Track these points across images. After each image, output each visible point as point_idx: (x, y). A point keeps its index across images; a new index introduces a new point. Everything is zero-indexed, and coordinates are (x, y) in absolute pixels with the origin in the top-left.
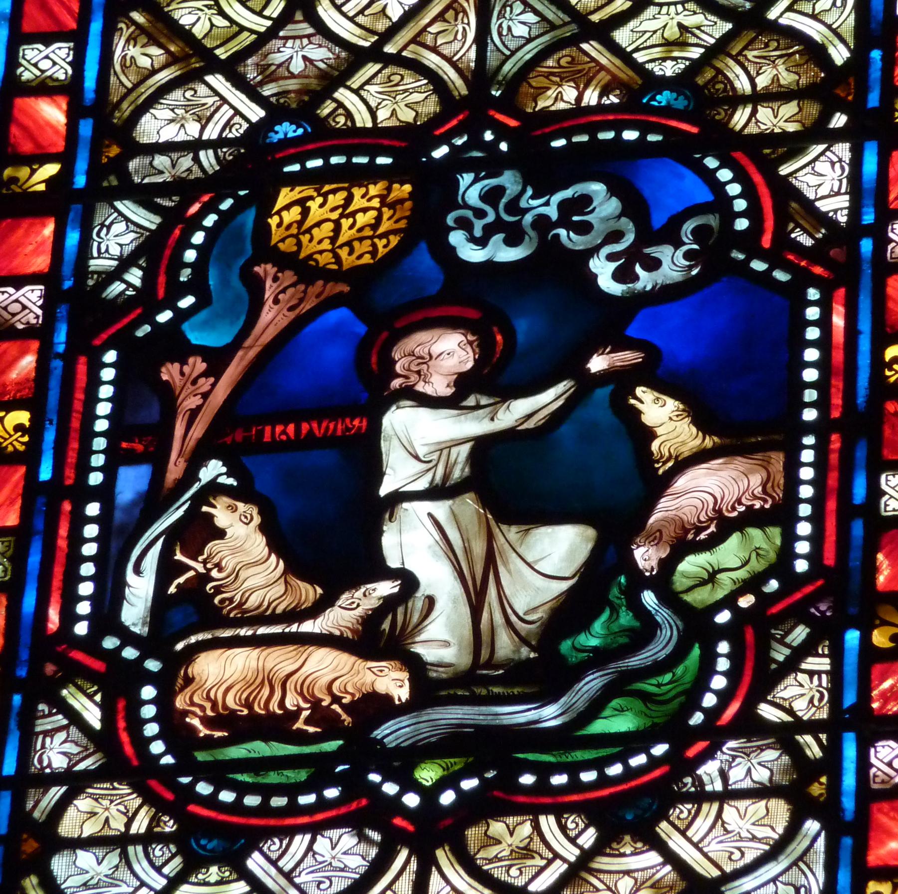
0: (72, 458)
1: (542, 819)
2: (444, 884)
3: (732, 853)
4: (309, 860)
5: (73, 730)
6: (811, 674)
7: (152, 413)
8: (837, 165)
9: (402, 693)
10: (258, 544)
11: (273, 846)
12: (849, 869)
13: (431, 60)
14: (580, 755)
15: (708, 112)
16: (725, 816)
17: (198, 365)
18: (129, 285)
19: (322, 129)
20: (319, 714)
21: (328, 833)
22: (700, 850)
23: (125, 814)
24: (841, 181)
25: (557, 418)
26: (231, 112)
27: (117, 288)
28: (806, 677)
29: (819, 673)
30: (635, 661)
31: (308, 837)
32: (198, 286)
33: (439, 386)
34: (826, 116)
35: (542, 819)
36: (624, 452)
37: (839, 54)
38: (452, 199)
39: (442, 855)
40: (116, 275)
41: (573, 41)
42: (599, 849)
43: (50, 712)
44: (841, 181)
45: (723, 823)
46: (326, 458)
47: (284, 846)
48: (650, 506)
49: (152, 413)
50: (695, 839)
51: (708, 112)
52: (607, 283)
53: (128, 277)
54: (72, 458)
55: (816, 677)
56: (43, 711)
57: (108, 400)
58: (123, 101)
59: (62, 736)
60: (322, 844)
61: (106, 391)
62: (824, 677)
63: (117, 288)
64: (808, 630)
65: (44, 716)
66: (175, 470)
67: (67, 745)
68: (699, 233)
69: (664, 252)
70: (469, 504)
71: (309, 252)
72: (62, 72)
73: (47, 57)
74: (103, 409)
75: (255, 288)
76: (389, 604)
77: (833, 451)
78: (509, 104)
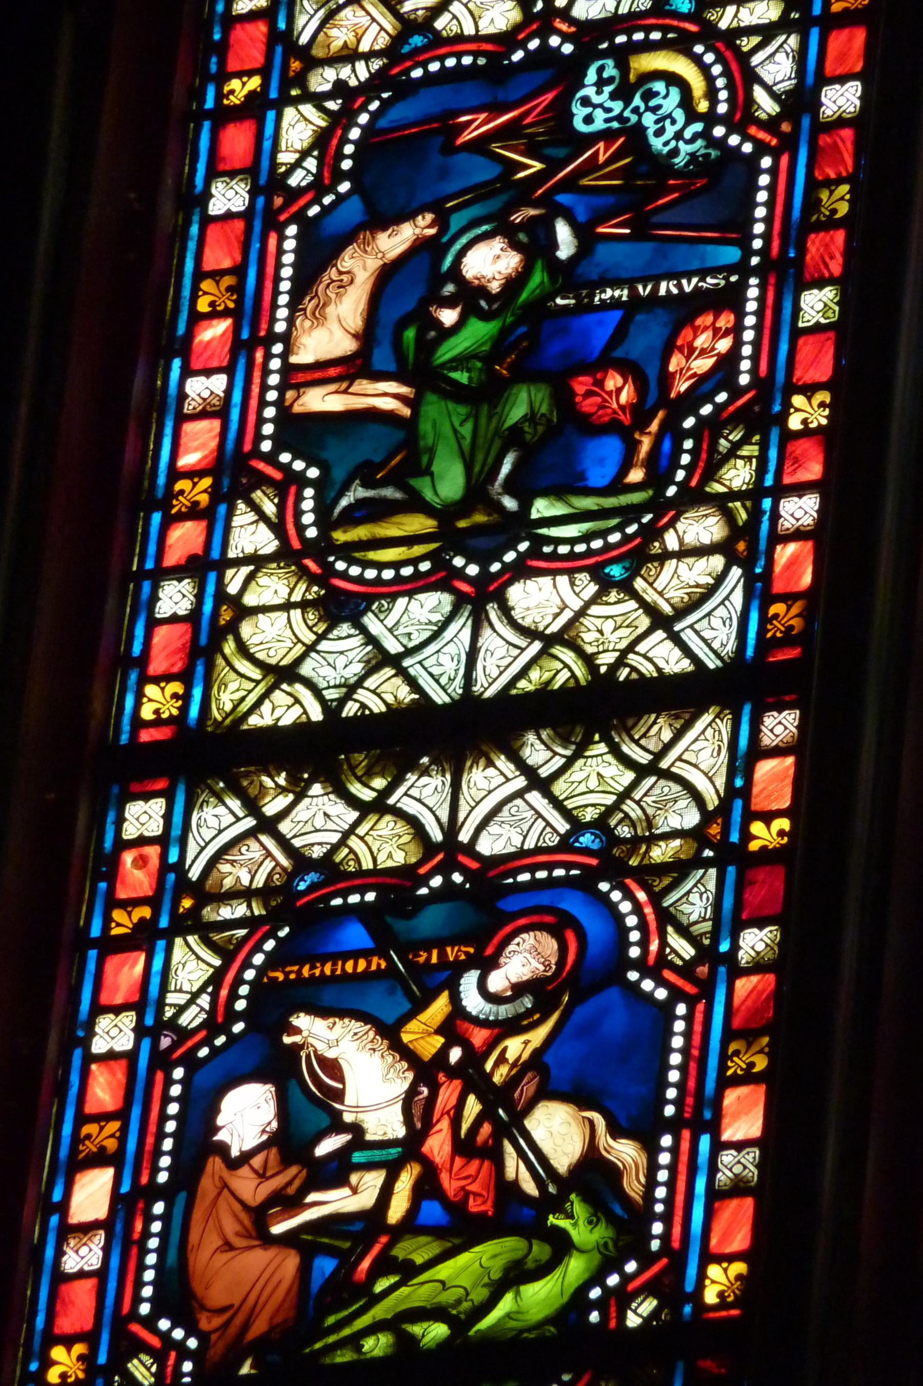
0: (688, 1112)
1: (371, 866)
2: (437, 813)
3: (247, 850)
4: (525, 827)
5: (685, 922)
6: (181, 991)
8: (705, 896)
11: (552, 840)
12: (140, 1107)
14: (443, 51)
16: (249, 877)
18: (726, 438)
21: (513, 850)
22: (537, 812)
23: (739, 20)
24: (706, 909)
26: (544, 824)
27: (736, 436)
28: (184, 989)
29: (176, 991)
31: (526, 847)
34: (700, 851)
35: (371, 866)
39: (437, 835)
40: (737, 446)
42: (595, 600)
43: (701, 938)
44: (706, 909)
45: (250, 872)
47: (542, 838)
50: (540, 820)
53: (728, 445)
54: (688, 1112)
55: (178, 988)
56: (706, 938)
57: (279, 320)
59: (694, 917)
60: (517, 841)
61: (762, 196)
62: (173, 989)
63: (736, 436)
64: (180, 1022)
65: (705, 933)
67: (690, 911)
73: (780, 723)
74: (679, 1026)
77: (147, 1168)
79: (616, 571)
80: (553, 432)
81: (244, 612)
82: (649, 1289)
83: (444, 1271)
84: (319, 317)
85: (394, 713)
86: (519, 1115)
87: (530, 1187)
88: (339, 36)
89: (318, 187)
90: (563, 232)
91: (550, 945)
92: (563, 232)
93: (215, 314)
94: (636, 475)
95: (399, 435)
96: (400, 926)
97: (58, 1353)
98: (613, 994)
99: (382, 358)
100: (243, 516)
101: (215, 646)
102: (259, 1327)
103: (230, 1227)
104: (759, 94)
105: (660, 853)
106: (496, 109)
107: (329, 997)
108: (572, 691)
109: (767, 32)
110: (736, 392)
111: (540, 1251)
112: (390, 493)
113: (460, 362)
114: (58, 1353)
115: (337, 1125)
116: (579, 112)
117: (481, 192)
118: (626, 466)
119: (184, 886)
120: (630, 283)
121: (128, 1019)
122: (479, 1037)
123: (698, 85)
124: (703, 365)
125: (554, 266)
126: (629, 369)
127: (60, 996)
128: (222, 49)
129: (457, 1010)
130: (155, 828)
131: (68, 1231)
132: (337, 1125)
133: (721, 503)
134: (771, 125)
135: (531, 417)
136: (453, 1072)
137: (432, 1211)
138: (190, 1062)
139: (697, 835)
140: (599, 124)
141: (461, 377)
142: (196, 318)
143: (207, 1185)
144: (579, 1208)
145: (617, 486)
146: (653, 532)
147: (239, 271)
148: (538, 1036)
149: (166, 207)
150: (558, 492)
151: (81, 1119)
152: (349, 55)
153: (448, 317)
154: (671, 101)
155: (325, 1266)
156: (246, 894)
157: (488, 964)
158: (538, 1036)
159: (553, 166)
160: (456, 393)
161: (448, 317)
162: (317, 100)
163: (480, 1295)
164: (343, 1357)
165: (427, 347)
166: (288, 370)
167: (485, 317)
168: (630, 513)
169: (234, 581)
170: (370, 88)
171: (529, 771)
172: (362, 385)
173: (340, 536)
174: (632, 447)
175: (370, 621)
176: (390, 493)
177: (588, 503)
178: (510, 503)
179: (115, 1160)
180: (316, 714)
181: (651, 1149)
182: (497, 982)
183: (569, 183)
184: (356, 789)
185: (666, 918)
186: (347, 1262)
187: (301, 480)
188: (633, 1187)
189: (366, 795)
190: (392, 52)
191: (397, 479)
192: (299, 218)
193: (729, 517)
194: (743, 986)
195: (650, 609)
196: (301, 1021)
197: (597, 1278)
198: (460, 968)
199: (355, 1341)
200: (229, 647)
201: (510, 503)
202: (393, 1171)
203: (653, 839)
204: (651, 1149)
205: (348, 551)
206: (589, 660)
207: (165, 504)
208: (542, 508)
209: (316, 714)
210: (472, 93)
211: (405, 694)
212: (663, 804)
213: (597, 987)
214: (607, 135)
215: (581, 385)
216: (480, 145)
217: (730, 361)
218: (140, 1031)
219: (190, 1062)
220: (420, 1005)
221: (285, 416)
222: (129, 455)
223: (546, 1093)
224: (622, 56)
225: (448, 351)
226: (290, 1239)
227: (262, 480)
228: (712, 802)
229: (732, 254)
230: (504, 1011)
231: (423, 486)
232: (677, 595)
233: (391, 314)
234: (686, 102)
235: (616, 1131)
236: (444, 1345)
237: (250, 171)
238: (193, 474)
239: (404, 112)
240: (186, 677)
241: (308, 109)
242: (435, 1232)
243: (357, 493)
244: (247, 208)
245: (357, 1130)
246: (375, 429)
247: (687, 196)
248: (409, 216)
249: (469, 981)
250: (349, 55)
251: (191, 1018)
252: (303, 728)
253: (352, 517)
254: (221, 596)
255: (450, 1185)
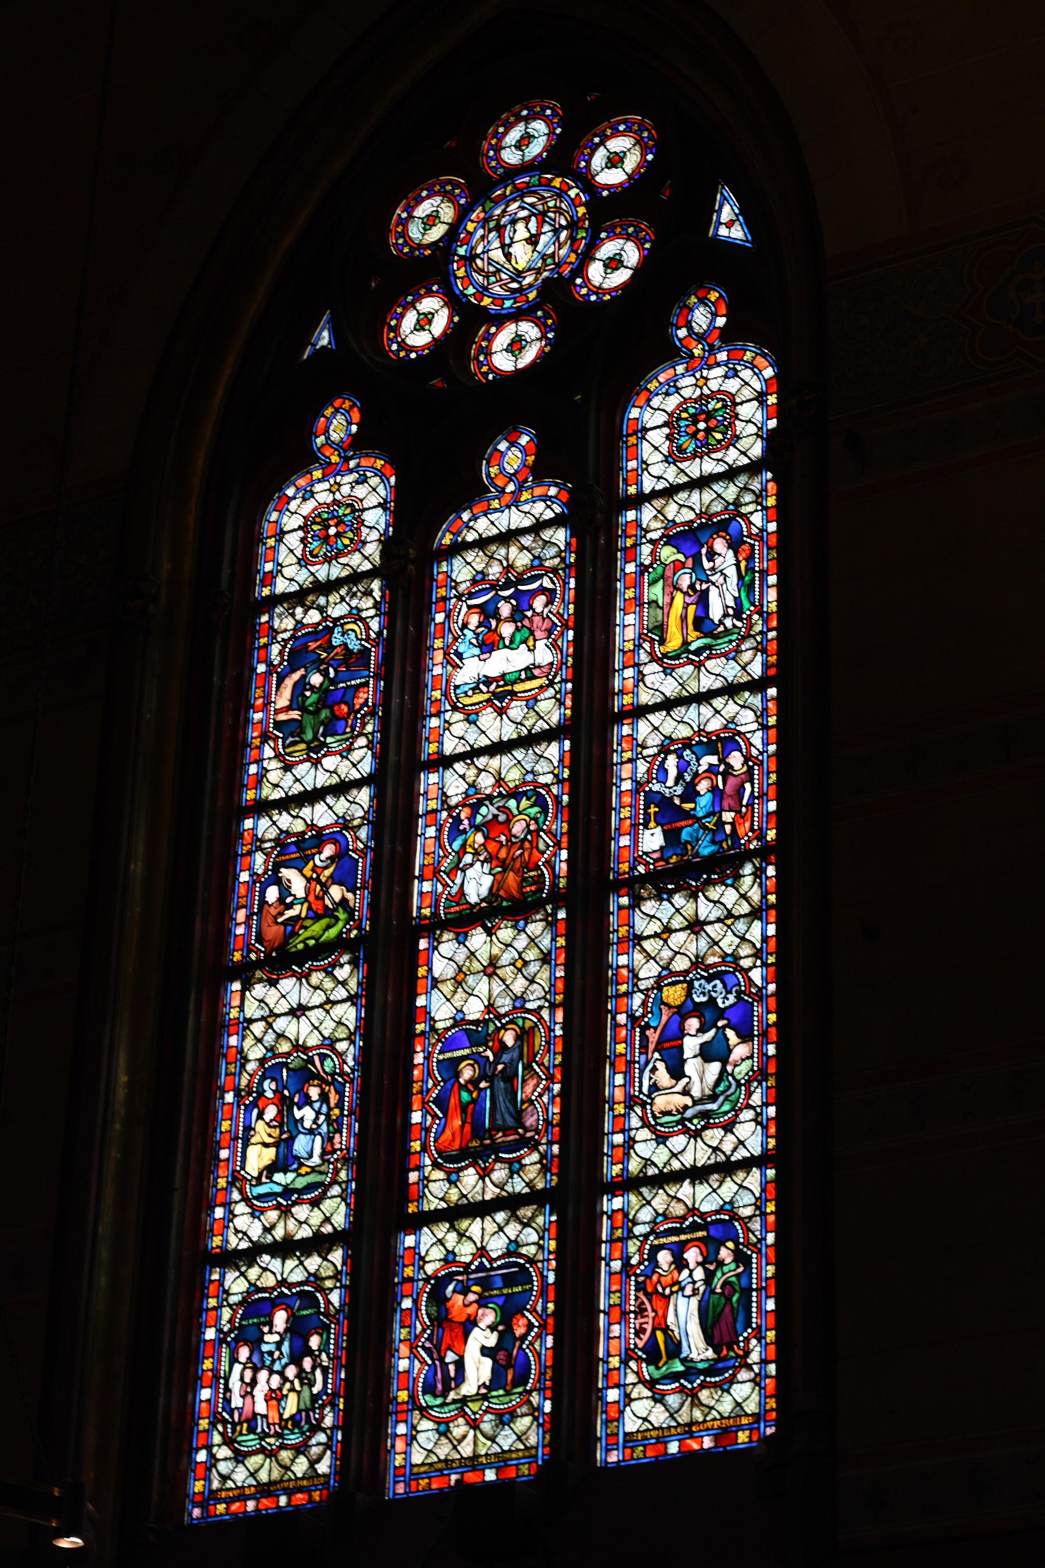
7: (644, 1043)
9: (690, 1103)
10: (665, 1071)
13: (688, 953)
15: (215, 1277)
17: (652, 1030)
19: (671, 972)
20: (677, 1110)
25: (714, 1038)
30: (729, 1093)
32: (651, 1012)
33: (693, 1032)
36: (725, 1043)
37: (758, 946)
38: (693, 987)
41: (711, 947)
46: (675, 1050)
48: (729, 1057)
49: (644, 1043)
51: (215, 1277)
52: (721, 1005)
58: (525, 528)
66: (650, 1056)
68: (736, 991)
69: (729, 996)
70: (699, 1059)
71: (759, 937)
72: (626, 963)
75: (661, 1010)
76: (688, 1083)
78: (702, 963)
79: (345, 754)
80: (331, 720)
81: (267, 771)
82: (356, 928)
83: (313, 928)
84: (281, 696)
85: (300, 793)
86: (327, 889)
87: (331, 906)
88: (283, 626)
89: (281, 663)
90: (331, 670)
91: (333, 847)
92: (331, 670)
93: (260, 697)
94: (348, 730)
95: (298, 724)
96: (302, 845)
97: (236, 953)
98: (346, 858)
99: (295, 706)
100: (267, 748)
101: (262, 780)
102: (276, 944)
103: (270, 921)
104: (371, 632)
105: (356, 823)
106: (316, 641)
107: (288, 864)
108: (337, 785)
109: (372, 617)
110: (368, 707)
111: (333, 921)
112: (297, 739)
113: (311, 705)
114: (236, 953)
115: (291, 895)
116: (334, 640)
117: (314, 662)
118: (346, 727)
119: (258, 840)
120: (345, 682)
121: (247, 873)
122: (319, 871)
123: (358, 632)
124: (361, 701)
125: (330, 679)
126: (346, 703)
127: (231, 869)
128: (258, 632)
129: (315, 865)
130: (251, 826)
131: (237, 924)
132: (291, 895)
133: (365, 735)
134: (374, 640)
135: (326, 718)
136: (314, 880)
137: (311, 914)
138: (260, 882)
139: (363, 818)
140: (338, 643)
141: (311, 708)
142: (255, 698)
143: (264, 912)
144: (341, 910)
145: (345, 733)
146: (352, 744)
147: (264, 687)
148: (331, 869)
149: (246, 673)
150: (332, 735)
151: (239, 897)
152: (286, 631)
153: (308, 694)
154: (352, 635)
155: (289, 928)
156: (270, 840)
157: (320, 853)
158: (331, 869)
159: (329, 654)
160: (310, 713)
161: (308, 694)
162: (278, 642)
163: (321, 932)
164: (294, 950)
165: (304, 702)
166: (275, 710)
167: (315, 693)
168: (347, 740)
169: (265, 764)
170: (290, 639)
171: (328, 805)
172: (291, 712)
173: (287, 750)
174: (347, 722)
175: (293, 771)
176: (297, 739)
177: (339, 738)
178: (322, 739)
179: (245, 907)
180: (284, 795)
181: (355, 894)
182: (323, 856)
183: (333, 659)
184: (292, 813)
185: (357, 838)
186: (294, 927)
187: (278, 737)
188: (351, 904)
189: (294, 814)
190: (295, 630)
191: (298, 736)
192: (277, 672)
193: (368, 738)
194: (281, 653)
195: (352, 763)
196: (282, 870)
197: (344, 927)
198: (314, 855)
199: (295, 946)
200: (265, 780)
201: (322, 739)
202: (302, 904)
203: (353, 820)
204: (355, 894)
205: (289, 754)
206: (339, 776)
207: (250, 746)
208: (329, 740)
209: (284, 795)
210: (312, 637)
211: (302, 789)
212: (356, 810)
213: (343, 856)
214: (340, 646)
215: (336, 708)
216: (313, 651)
217: (367, 700)
218: (250, 875)
219: (260, 882)
220: (307, 864)
221: (276, 722)
222: (241, 736)
223: (334, 883)
224: (342, 625)
225: (308, 702)
226: (282, 923)
227: (270, 738)
228: (366, 809)
229: (366, 673)
230: (324, 864)
231: (303, 736)
232: (358, 759)
233: (295, 695)
234: (356, 637)
235: (348, 891)
236: (314, 945)
237: (265, 661)
238: (256, 738)
239: (298, 643)
240: (256, 789)
241: (635, 1240)
242: (311, 918)
243: (291, 739)
244: (517, 372)
245: (294, 895)
246: (293, 723)
247: (357, 659)
248: (299, 669)
249: (317, 857)
250: (286, 631)
251: (260, 872)
252: (281, 799)
253: (290, 746)
254: (263, 768)
255: (314, 907)
